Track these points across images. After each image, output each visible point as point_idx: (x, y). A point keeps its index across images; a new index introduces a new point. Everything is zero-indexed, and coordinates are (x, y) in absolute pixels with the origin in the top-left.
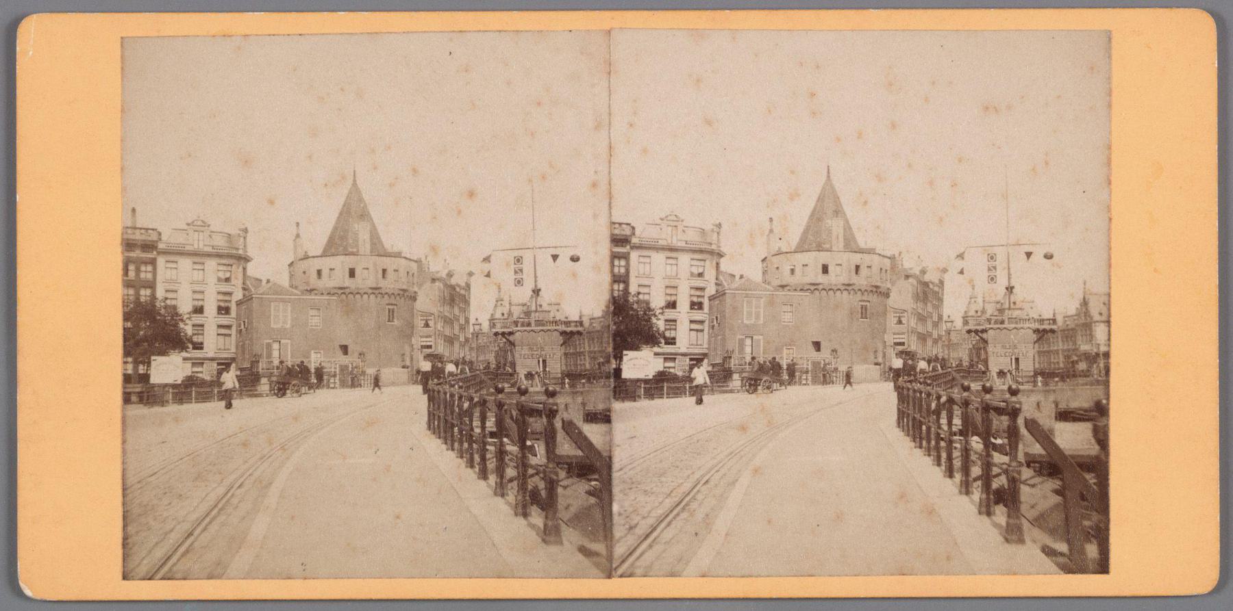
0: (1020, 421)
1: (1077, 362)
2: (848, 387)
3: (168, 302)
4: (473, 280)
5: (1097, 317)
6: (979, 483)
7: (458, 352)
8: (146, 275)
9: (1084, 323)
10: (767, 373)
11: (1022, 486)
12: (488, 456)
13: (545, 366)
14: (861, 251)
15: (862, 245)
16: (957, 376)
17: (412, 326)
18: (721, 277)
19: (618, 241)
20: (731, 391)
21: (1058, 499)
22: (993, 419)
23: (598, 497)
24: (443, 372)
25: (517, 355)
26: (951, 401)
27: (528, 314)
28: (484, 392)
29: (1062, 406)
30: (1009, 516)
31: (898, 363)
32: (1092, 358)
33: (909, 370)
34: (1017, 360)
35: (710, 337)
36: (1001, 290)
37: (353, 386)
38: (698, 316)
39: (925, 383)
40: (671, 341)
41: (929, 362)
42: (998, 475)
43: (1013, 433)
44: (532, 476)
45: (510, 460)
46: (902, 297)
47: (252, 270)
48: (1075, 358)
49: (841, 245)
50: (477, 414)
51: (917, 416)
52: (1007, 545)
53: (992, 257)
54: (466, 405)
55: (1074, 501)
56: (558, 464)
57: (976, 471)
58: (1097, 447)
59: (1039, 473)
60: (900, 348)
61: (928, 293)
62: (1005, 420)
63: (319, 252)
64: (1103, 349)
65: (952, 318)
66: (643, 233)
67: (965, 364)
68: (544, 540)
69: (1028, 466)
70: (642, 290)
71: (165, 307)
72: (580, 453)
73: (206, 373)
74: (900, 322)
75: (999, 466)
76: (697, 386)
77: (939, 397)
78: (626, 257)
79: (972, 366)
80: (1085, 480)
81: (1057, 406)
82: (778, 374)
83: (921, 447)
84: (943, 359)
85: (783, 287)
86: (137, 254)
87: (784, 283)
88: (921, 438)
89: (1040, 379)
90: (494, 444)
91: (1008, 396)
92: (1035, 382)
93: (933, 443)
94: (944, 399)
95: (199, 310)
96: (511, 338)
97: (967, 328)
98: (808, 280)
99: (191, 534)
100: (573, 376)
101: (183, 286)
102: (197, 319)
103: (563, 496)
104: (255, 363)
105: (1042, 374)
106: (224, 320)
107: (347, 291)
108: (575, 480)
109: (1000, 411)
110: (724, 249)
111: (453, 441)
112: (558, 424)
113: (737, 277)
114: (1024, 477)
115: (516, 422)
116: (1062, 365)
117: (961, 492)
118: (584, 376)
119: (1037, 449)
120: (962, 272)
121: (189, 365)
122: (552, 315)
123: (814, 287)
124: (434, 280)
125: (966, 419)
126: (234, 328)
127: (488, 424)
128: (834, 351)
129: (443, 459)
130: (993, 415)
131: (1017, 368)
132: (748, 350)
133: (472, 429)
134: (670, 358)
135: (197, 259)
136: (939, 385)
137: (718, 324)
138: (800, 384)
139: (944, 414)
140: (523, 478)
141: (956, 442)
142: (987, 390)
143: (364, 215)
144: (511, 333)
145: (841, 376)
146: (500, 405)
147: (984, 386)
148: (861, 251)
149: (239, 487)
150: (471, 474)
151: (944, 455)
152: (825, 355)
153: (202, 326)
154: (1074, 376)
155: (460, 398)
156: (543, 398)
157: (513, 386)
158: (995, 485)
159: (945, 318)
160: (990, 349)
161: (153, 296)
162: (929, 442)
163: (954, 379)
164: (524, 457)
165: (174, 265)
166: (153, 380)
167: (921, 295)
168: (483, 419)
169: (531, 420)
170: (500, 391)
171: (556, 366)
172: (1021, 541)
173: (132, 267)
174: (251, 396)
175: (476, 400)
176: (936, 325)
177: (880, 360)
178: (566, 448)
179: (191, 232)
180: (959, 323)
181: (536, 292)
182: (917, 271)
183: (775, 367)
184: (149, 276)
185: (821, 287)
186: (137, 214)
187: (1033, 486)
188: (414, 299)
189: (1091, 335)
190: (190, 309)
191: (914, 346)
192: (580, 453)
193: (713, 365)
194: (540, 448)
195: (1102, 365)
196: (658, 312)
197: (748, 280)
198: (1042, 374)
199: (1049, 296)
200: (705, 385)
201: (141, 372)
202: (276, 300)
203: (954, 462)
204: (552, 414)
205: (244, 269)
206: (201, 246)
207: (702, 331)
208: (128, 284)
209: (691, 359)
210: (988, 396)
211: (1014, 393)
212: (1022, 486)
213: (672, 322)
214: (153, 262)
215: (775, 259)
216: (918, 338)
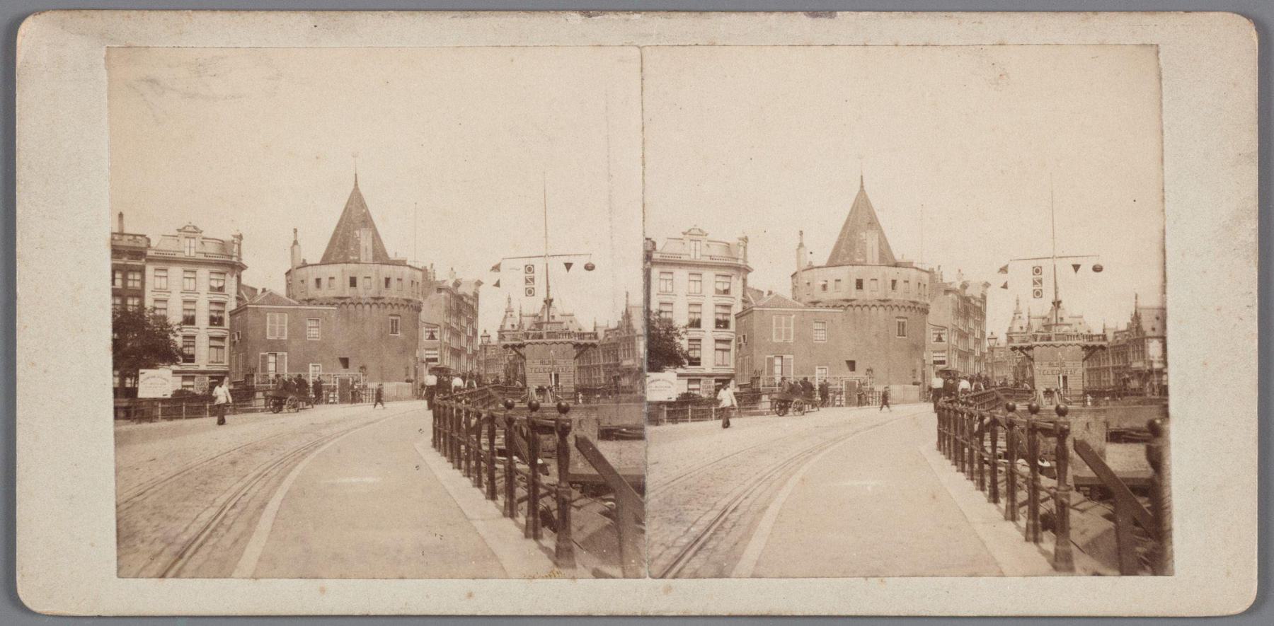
0: (1069, 443)
1: (1128, 380)
3: (663, 315)
4: (481, 288)
5: (1150, 333)
6: (1026, 508)
7: (466, 365)
8: (134, 282)
9: (1135, 338)
10: (797, 394)
11: (1072, 511)
12: (497, 475)
13: (557, 381)
15: (898, 258)
16: (1001, 395)
17: (415, 339)
20: (761, 414)
21: (1111, 524)
22: (1042, 440)
23: (613, 518)
24: (956, 389)
25: (527, 369)
26: (995, 422)
28: (492, 407)
29: (1113, 426)
30: (1057, 543)
31: (938, 383)
32: (1144, 376)
33: (949, 390)
34: (1065, 378)
35: (231, 353)
36: (541, 304)
38: (723, 334)
39: (966, 403)
40: (695, 362)
41: (971, 381)
42: (1046, 500)
43: (1061, 457)
44: (544, 496)
45: (521, 479)
46: (433, 311)
47: (753, 281)
48: (1129, 374)
49: (370, 256)
50: (485, 431)
51: (959, 438)
53: (1037, 271)
54: (474, 421)
55: (1139, 528)
56: (571, 484)
57: (1022, 496)
58: (1151, 470)
59: (1090, 497)
60: (941, 367)
61: (971, 309)
62: (1052, 442)
64: (1157, 366)
65: (995, 335)
68: (556, 564)
69: (1078, 490)
70: (664, 308)
72: (594, 472)
73: (197, 387)
74: (432, 337)
75: (1048, 490)
76: (723, 409)
77: (982, 419)
79: (1017, 385)
82: (306, 394)
83: (963, 471)
84: (986, 378)
86: (124, 260)
89: (1089, 398)
90: (503, 462)
91: (1056, 416)
92: (1085, 401)
93: (976, 466)
94: (987, 420)
95: (696, 324)
96: (1030, 353)
97: (503, 343)
98: (841, 296)
99: (181, 557)
100: (587, 391)
101: (173, 295)
103: (577, 516)
104: (755, 379)
105: (1092, 393)
106: (217, 332)
107: (348, 301)
108: (589, 500)
109: (1047, 432)
110: (245, 260)
111: (460, 459)
112: (571, 441)
113: (765, 294)
114: (1073, 501)
115: (526, 438)
116: (1112, 383)
118: (598, 391)
119: (1087, 472)
122: (1073, 328)
123: (340, 301)
125: (1011, 441)
126: (733, 342)
127: (497, 441)
128: (870, 370)
131: (1065, 386)
132: (777, 370)
133: (480, 447)
135: (668, 269)
136: (982, 405)
137: (746, 342)
138: (327, 402)
139: (987, 436)
140: (533, 498)
141: (1000, 465)
142: (1034, 411)
143: (873, 223)
144: (1030, 348)
145: (878, 399)
146: (1011, 425)
147: (1030, 406)
148: (896, 265)
149: (234, 506)
151: (988, 479)
152: (859, 375)
153: (194, 337)
154: (1126, 394)
155: (467, 413)
156: (556, 414)
157: (523, 401)
158: (1043, 509)
159: (988, 335)
160: (1036, 367)
161: (142, 306)
162: (972, 466)
163: (998, 399)
164: (535, 476)
165: (163, 274)
166: (141, 395)
167: (455, 308)
168: (492, 436)
169: (543, 437)
171: (569, 381)
172: (1070, 570)
173: (118, 275)
174: (752, 415)
175: (484, 415)
176: (978, 342)
177: (919, 379)
178: (580, 466)
179: (182, 239)
180: (1003, 340)
181: (549, 302)
183: (807, 387)
184: (137, 284)
185: (854, 303)
186: (125, 218)
187: (1082, 511)
188: (419, 309)
191: (954, 365)
192: (594, 472)
193: (741, 387)
194: (553, 468)
197: (777, 296)
198: (1092, 393)
199: (1100, 310)
200: (227, 405)
201: (128, 385)
202: (270, 310)
203: (999, 486)
204: (564, 431)
205: (745, 280)
208: (115, 293)
209: (717, 381)
210: (1034, 417)
211: (1061, 412)
212: (1072, 511)
213: (190, 339)
214: (142, 271)
215: (806, 274)
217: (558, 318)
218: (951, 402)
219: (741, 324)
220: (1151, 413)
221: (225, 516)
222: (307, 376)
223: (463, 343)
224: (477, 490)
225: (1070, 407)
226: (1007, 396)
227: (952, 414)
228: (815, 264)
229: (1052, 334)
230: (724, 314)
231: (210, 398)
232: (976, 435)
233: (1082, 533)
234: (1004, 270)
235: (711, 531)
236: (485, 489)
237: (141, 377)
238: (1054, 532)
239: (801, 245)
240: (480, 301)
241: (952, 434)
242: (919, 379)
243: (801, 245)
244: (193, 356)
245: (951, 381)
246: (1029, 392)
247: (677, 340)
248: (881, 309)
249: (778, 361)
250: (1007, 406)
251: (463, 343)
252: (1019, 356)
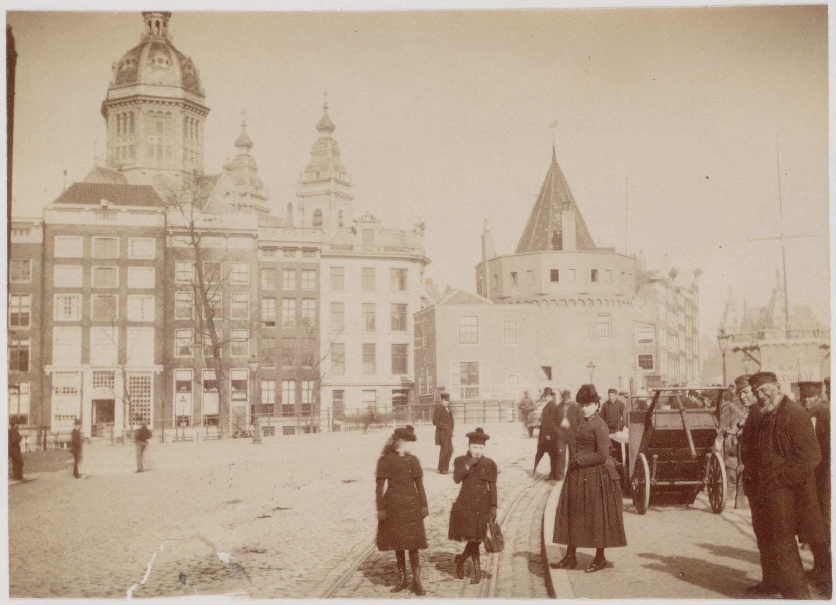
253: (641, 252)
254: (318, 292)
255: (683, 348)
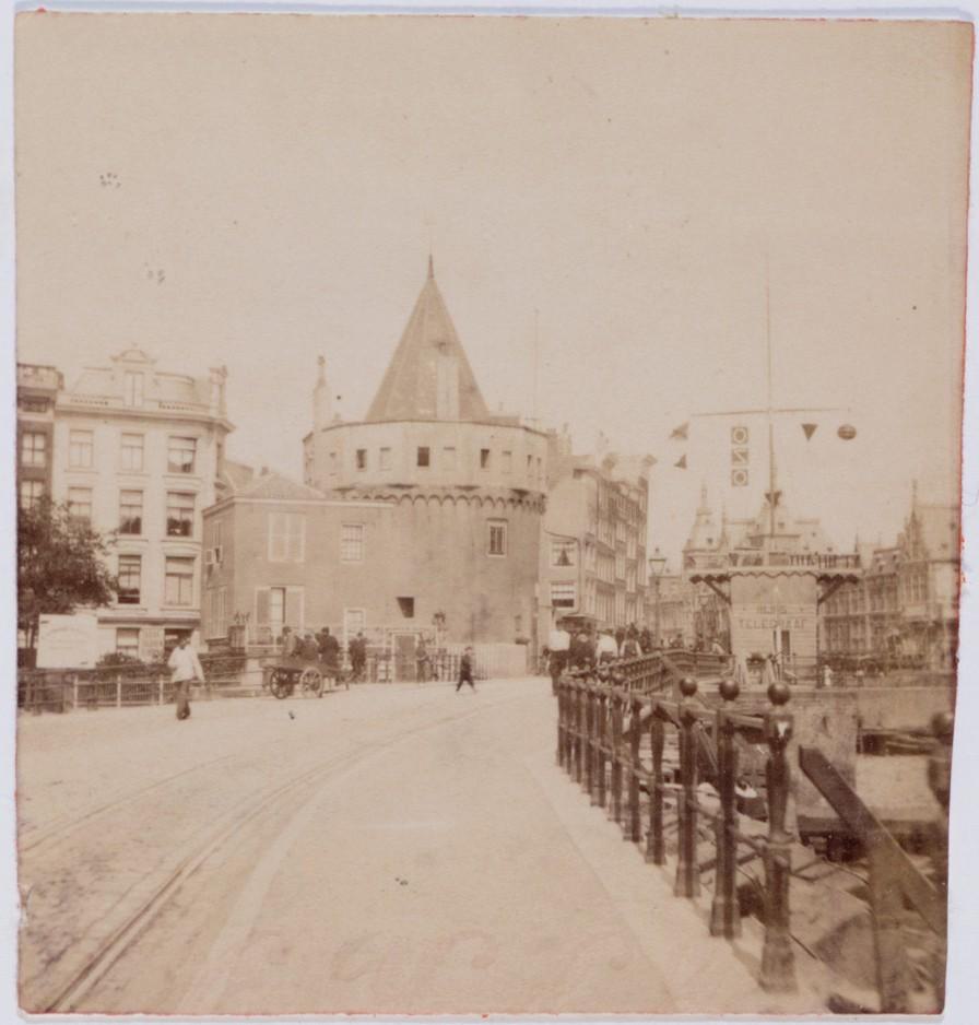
0: (791, 755)
1: (898, 640)
2: (466, 686)
3: (74, 511)
5: (936, 554)
6: (712, 874)
10: (309, 658)
11: (793, 881)
14: (493, 422)
18: (226, 473)
19: (28, 400)
24: (591, 654)
26: (660, 714)
27: (757, 540)
30: (767, 940)
31: (560, 640)
33: (579, 655)
34: (786, 635)
35: (204, 588)
36: (758, 501)
37: (421, 677)
38: (180, 546)
40: (130, 597)
41: (619, 637)
43: (775, 777)
46: (568, 512)
47: (236, 448)
52: (762, 993)
53: (740, 434)
57: (706, 850)
59: (827, 854)
60: (565, 611)
61: (620, 507)
63: (361, 417)
64: (948, 614)
65: (663, 554)
66: (80, 385)
67: (689, 642)
68: (762, 984)
69: (805, 841)
70: (77, 497)
71: (69, 520)
73: (145, 648)
74: (564, 561)
75: (749, 842)
76: (179, 684)
77: (637, 707)
78: (46, 433)
79: (700, 645)
80: (911, 868)
81: (860, 724)
83: (602, 805)
84: (646, 634)
85: (343, 490)
87: (346, 483)
88: (602, 786)
89: (828, 672)
91: (768, 705)
93: (625, 795)
94: (646, 711)
97: (692, 572)
101: (100, 482)
102: (129, 544)
109: (752, 734)
110: (232, 417)
113: (257, 474)
116: (869, 647)
117: (676, 893)
119: (822, 810)
120: (682, 464)
121: (111, 631)
122: (802, 542)
123: (402, 491)
124: (578, 472)
128: (440, 616)
129: (586, 825)
130: (738, 741)
134: (129, 628)
135: (132, 427)
136: (638, 683)
138: (375, 678)
139: (646, 740)
141: (668, 793)
142: (729, 694)
144: (723, 579)
146: (688, 719)
147: (722, 687)
148: (493, 422)
150: (633, 854)
151: (645, 821)
152: (421, 623)
153: (138, 557)
154: (894, 667)
158: (741, 878)
159: (650, 553)
160: (736, 613)
167: (605, 507)
168: (658, 749)
170: (689, 691)
176: (633, 566)
177: (527, 634)
180: (676, 563)
182: (597, 462)
183: (328, 646)
184: (39, 458)
189: (925, 587)
190: (115, 524)
193: (211, 643)
195: (946, 646)
196: (106, 539)
199: (852, 518)
200: (195, 682)
203: (665, 833)
204: (778, 745)
205: (219, 446)
206: (138, 402)
207: (189, 576)
209: (168, 632)
210: (730, 706)
211: (778, 698)
216: (600, 591)
217: (790, 529)
218: (583, 676)
219: (205, 528)
220: (932, 701)
221: (179, 890)
222: (340, 630)
223: (620, 571)
224: (631, 845)
225: (793, 688)
226: (682, 667)
227: (584, 699)
228: (347, 418)
229: (764, 553)
230: (183, 510)
231: (163, 669)
232: (626, 736)
233: (812, 922)
234: (680, 433)
235: (153, 911)
236: (644, 845)
237: (42, 629)
238: (762, 919)
239: (321, 382)
240: (651, 494)
241: (583, 736)
242: (527, 634)
243: (321, 382)
244: (136, 591)
245: (583, 638)
246: (722, 659)
247: (98, 555)
248: (462, 502)
249: (277, 598)
250: (682, 683)
251: (620, 571)
252: (706, 592)
253: (566, 426)
254: (48, 469)
255: (621, 576)
